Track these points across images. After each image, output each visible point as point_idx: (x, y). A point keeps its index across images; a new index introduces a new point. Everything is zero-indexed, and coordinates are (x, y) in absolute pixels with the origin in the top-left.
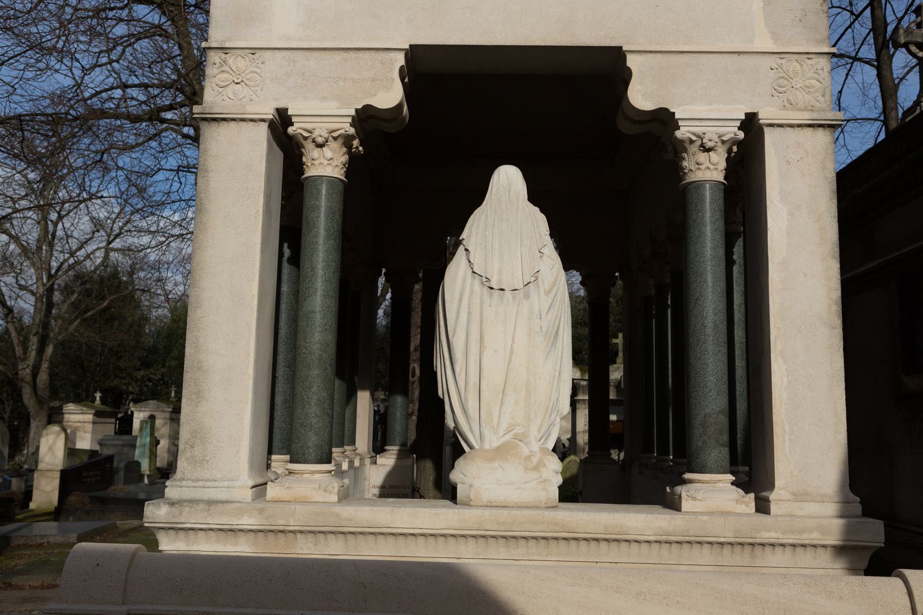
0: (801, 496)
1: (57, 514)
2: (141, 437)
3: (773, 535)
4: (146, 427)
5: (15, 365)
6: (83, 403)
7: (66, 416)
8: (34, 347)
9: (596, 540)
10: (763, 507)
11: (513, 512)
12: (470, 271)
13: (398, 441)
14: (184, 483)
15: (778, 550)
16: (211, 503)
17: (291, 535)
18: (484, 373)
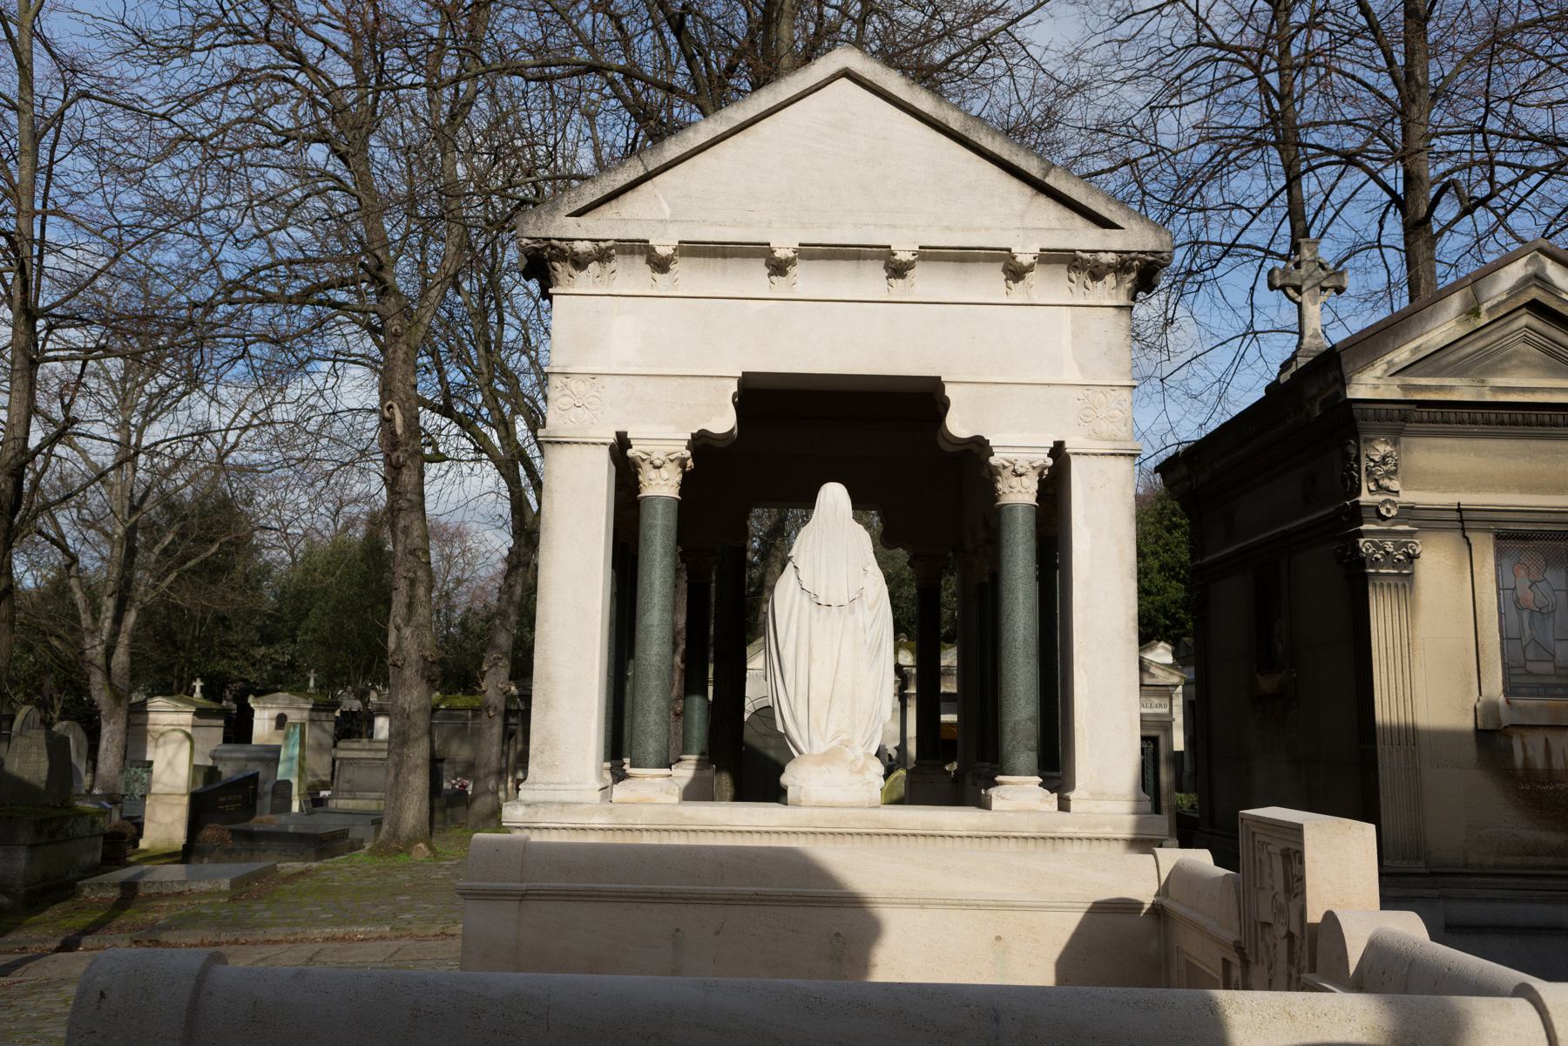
0: (1098, 796)
1: (187, 854)
2: (286, 746)
3: (1072, 830)
4: (294, 733)
5: (78, 644)
6: (177, 697)
7: (152, 716)
8: (109, 614)
9: (914, 835)
10: (1064, 806)
11: (840, 811)
12: (799, 587)
13: (695, 749)
14: (536, 786)
15: (1077, 843)
16: (563, 804)
17: (637, 833)
18: (812, 683)
